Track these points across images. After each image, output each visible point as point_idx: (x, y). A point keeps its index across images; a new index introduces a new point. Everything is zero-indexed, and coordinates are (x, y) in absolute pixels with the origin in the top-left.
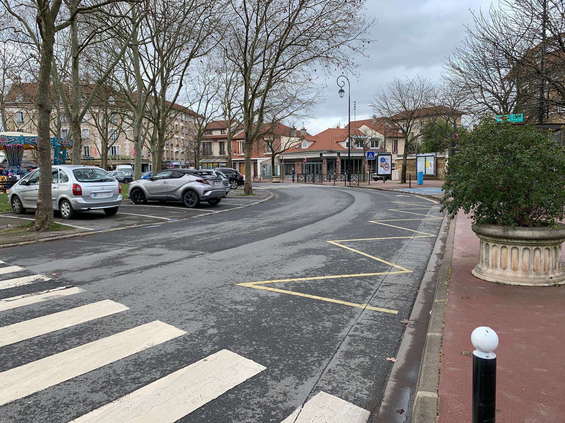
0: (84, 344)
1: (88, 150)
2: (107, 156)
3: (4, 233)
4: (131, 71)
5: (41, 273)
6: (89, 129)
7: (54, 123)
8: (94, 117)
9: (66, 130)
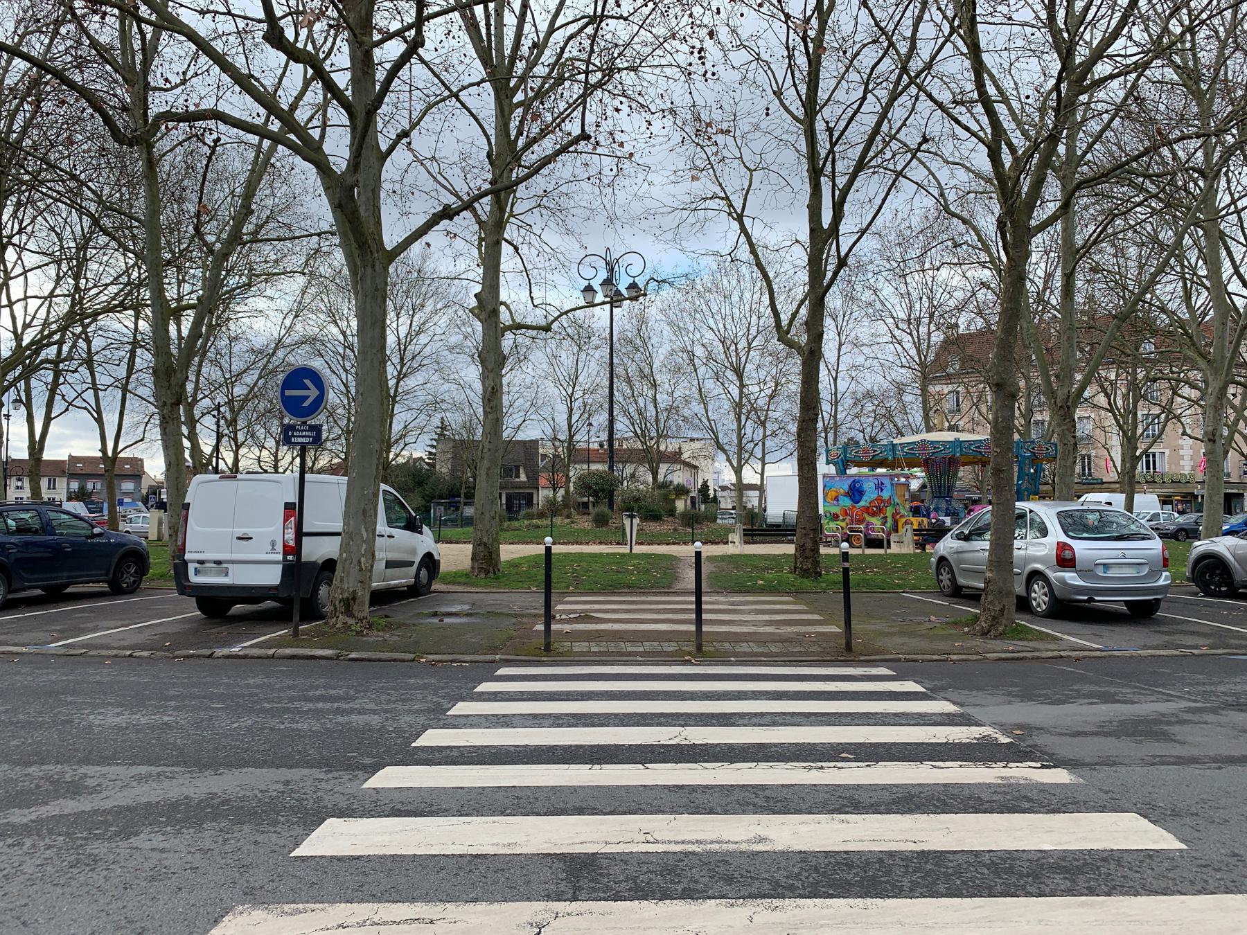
0: (1082, 895)
1: (1089, 463)
2: (1134, 476)
3: (924, 632)
4: (1199, 277)
5: (993, 724)
6: (1093, 416)
7: (1019, 408)
8: (1104, 390)
9: (1043, 422)
